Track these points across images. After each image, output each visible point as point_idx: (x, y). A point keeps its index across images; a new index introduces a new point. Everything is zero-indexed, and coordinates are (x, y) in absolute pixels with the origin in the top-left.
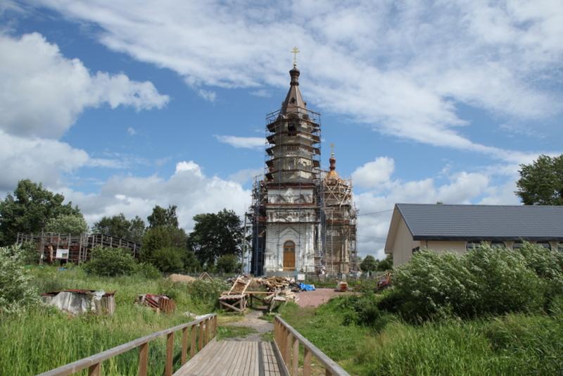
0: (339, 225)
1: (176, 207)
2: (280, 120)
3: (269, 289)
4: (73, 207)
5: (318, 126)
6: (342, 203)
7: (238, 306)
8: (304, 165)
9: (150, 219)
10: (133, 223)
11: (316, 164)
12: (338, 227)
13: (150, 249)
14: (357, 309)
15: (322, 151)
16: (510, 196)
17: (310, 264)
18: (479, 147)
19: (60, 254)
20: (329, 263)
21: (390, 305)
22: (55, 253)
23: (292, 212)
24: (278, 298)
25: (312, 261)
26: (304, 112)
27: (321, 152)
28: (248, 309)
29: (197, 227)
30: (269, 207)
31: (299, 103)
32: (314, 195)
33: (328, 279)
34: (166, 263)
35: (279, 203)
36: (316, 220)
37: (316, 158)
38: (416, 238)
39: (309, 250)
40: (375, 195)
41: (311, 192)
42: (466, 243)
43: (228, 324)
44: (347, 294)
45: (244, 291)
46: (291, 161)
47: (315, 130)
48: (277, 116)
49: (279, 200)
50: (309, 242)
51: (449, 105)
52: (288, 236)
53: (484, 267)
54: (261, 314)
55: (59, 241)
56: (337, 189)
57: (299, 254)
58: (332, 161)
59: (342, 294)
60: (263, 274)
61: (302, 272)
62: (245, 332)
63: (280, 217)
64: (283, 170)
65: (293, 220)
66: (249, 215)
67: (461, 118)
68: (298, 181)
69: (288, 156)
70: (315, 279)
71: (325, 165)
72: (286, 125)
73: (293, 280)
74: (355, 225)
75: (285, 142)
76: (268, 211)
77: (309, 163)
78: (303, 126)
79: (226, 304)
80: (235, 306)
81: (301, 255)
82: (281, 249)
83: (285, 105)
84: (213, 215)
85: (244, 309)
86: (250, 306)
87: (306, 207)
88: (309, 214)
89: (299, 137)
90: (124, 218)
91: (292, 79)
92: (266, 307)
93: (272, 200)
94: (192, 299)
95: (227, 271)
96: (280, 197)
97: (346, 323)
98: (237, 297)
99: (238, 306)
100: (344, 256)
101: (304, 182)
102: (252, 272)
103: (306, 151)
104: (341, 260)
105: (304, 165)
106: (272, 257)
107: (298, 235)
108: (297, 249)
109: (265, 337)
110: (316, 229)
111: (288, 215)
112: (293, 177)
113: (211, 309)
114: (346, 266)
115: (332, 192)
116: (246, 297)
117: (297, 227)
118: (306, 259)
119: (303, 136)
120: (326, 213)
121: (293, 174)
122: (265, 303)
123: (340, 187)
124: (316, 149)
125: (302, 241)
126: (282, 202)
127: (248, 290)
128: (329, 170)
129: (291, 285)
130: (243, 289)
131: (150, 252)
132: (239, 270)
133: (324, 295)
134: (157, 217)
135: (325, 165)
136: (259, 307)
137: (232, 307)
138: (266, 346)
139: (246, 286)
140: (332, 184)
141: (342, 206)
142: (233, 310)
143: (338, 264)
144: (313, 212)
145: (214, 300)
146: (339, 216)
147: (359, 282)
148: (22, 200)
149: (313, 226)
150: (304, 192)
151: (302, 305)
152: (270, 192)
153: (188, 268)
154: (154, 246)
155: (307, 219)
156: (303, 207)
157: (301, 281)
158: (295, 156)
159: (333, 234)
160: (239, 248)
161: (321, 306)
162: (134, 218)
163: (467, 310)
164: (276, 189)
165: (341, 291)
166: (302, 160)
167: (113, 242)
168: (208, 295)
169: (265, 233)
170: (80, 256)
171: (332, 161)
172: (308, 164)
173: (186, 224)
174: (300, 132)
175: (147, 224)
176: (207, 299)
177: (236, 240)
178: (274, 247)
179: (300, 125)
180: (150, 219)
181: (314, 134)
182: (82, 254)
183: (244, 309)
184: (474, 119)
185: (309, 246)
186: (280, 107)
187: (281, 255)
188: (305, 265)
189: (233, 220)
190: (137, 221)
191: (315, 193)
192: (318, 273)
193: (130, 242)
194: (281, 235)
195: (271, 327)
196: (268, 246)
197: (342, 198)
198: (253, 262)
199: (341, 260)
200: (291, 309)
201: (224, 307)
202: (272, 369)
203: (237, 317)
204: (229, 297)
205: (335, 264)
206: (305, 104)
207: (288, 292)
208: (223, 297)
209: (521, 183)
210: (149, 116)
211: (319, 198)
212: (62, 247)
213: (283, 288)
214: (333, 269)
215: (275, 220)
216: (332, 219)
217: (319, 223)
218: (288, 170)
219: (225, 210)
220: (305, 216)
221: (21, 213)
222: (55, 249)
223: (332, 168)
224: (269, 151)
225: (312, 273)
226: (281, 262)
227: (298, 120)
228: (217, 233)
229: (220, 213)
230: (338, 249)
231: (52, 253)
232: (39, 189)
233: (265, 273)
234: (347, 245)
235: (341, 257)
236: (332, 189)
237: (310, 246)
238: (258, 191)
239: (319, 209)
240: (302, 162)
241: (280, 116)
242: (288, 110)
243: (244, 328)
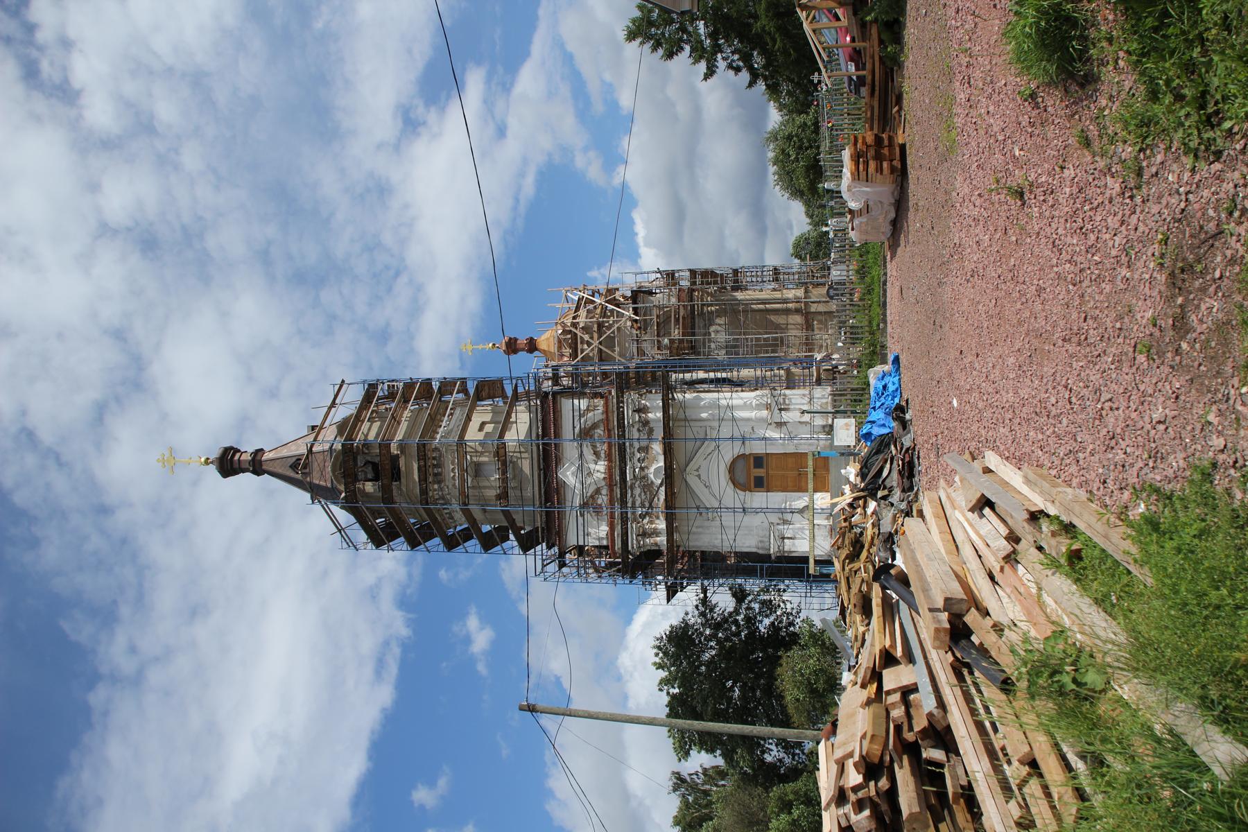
0: (693, 320)
6: (629, 313)
25: (797, 397)
39: (758, 407)
41: (567, 405)
49: (598, 510)
50: (731, 408)
52: (711, 478)
57: (774, 441)
58: (512, 347)
61: (829, 430)
81: (773, 434)
82: (758, 499)
88: (641, 410)
89: (402, 446)
100: (785, 301)
104: (797, 311)
108: (758, 448)
111: (645, 477)
112: (526, 466)
118: (786, 416)
119: (399, 435)
125: (726, 431)
126: (603, 499)
141: (636, 311)
144: (631, 397)
150: (568, 428)
159: (719, 334)
164: (561, 515)
172: (488, 417)
178: (742, 523)
185: (745, 407)
187: (776, 499)
199: (797, 311)
205: (809, 326)
220: (646, 423)
235: (787, 312)
237: (745, 405)
240: (481, 436)
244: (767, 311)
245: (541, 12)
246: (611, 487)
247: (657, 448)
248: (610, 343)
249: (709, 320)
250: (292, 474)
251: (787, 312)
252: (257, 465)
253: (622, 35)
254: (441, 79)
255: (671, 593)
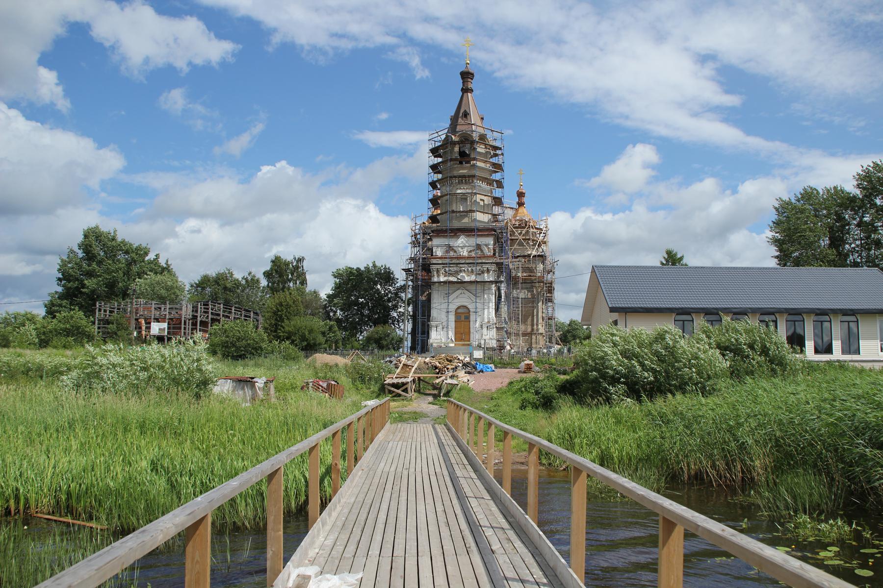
0: (529, 283)
1: (303, 258)
2: (447, 142)
3: (440, 371)
4: (162, 262)
5: (500, 149)
6: (534, 253)
7: (406, 391)
8: (482, 203)
9: (267, 275)
10: (244, 282)
11: (498, 201)
12: (529, 285)
13: (276, 320)
14: (537, 393)
15: (505, 184)
16: (754, 249)
17: (490, 337)
18: (755, 142)
19: (156, 328)
20: (517, 335)
21: (567, 388)
22: (148, 328)
23: (465, 267)
24: (449, 381)
25: (493, 333)
26: (481, 131)
27: (505, 185)
28: (416, 394)
29: (338, 288)
30: (434, 261)
31: (474, 118)
32: (495, 244)
33: (513, 357)
34: (303, 338)
35: (448, 255)
36: (498, 277)
37: (498, 193)
38: (613, 310)
39: (489, 318)
40: (587, 232)
41: (490, 241)
42: (674, 315)
43: (397, 409)
44: (529, 376)
45: (411, 374)
46: (464, 198)
47: (496, 155)
48: (443, 137)
49: (447, 252)
50: (488, 308)
51: (709, 70)
52: (460, 299)
53: (666, 348)
54: (431, 399)
55: (154, 313)
56: (527, 232)
57: (475, 324)
58: (521, 195)
59: (524, 375)
60: (428, 350)
61: (479, 346)
62: (416, 417)
63: (451, 275)
64: (453, 212)
65: (467, 279)
66: (407, 271)
67: (727, 92)
68: (473, 225)
69: (459, 191)
70: (497, 357)
71: (510, 200)
72: (457, 149)
73: (468, 359)
74: (551, 283)
75: (456, 173)
76: (433, 267)
77: (488, 200)
78: (479, 150)
79: (392, 389)
80: (403, 391)
81: (478, 325)
82: (452, 317)
83: (454, 120)
84: (358, 269)
85: (412, 394)
86: (418, 391)
87: (484, 261)
88: (488, 271)
89: (474, 165)
90: (232, 274)
91: (463, 82)
92: (436, 392)
93: (439, 252)
94: (353, 384)
95: (381, 347)
96: (450, 248)
97: (523, 407)
98: (404, 380)
99: (406, 391)
100: (537, 325)
101: (481, 226)
102: (413, 348)
103: (484, 185)
104: (533, 330)
105: (482, 203)
106: (440, 328)
107: (473, 298)
108: (472, 318)
109: (436, 421)
110: (499, 289)
111: (461, 271)
112: (466, 220)
113: (375, 395)
114: (540, 337)
115: (520, 237)
116: (414, 381)
117: (472, 287)
118: (485, 330)
119: (479, 164)
120: (511, 266)
121: (466, 216)
122: (435, 387)
123: (531, 230)
124: (497, 181)
125: (479, 305)
126: (452, 254)
127: (415, 373)
128: (515, 206)
129: (465, 365)
130: (409, 373)
131: (276, 325)
132: (397, 344)
133: (508, 375)
134: (276, 271)
135: (510, 200)
136: (428, 392)
137: (399, 391)
138: (440, 429)
139: (413, 369)
140: (520, 227)
141: (535, 256)
142: (399, 395)
143: (528, 335)
144: (494, 267)
145: (378, 385)
146: (531, 270)
147: (553, 360)
148: (90, 256)
149: (493, 287)
150: (481, 241)
151: (478, 389)
152: (436, 241)
153: (334, 347)
154: (281, 317)
155: (487, 277)
156: (480, 261)
157: (477, 360)
158: (470, 191)
159: (523, 294)
160: (395, 315)
161: (499, 390)
162: (246, 275)
163: (636, 389)
164: (444, 237)
165: (525, 372)
166: (479, 197)
167: (224, 311)
168: (370, 379)
169: (429, 295)
170: (183, 331)
171: (521, 195)
172: (486, 202)
173: (321, 284)
174: (474, 159)
175: (264, 283)
176: (369, 384)
177: (390, 304)
178: (442, 311)
179: (475, 149)
180: (267, 275)
181: (494, 160)
182: (185, 329)
183: (412, 394)
184: (752, 95)
185: (489, 312)
186: (447, 124)
187: (452, 325)
188: (484, 337)
189: (387, 277)
190: (249, 278)
191: (497, 240)
192: (502, 348)
193: (246, 310)
194: (451, 297)
195: (443, 412)
196: (434, 313)
197: (534, 245)
198: (414, 332)
199: (533, 330)
200: (464, 393)
201: (390, 392)
202: (450, 443)
203: (405, 402)
204: (395, 381)
205: (524, 335)
206: (482, 119)
207: (461, 374)
208: (388, 381)
209: (777, 224)
210: (200, 79)
211: (502, 249)
212: (157, 320)
213: (455, 369)
214: (521, 342)
215: (442, 279)
216: (520, 274)
217: (501, 282)
218: (460, 212)
219: (374, 266)
220: (483, 272)
221: (90, 274)
222: (148, 323)
223: (521, 204)
224: (433, 185)
225: (493, 349)
226: (451, 335)
227: (473, 142)
228: (364, 300)
229: (367, 268)
230: (529, 315)
231: (144, 328)
232: (113, 239)
233: (431, 349)
234: (541, 309)
235: (532, 325)
236: (520, 234)
237: (490, 313)
238: (418, 236)
239: (502, 263)
240: (478, 200)
241: (447, 137)
242: (459, 128)
243: (415, 413)
244: (533, 316)
245: (777, 144)
246: (458, 258)
247: (473, 278)
248: (521, 244)
249: (530, 290)
250: (462, 111)
251: (532, 325)
252: (466, 90)
253: (671, 247)
254: (731, 76)
255: (407, 271)
